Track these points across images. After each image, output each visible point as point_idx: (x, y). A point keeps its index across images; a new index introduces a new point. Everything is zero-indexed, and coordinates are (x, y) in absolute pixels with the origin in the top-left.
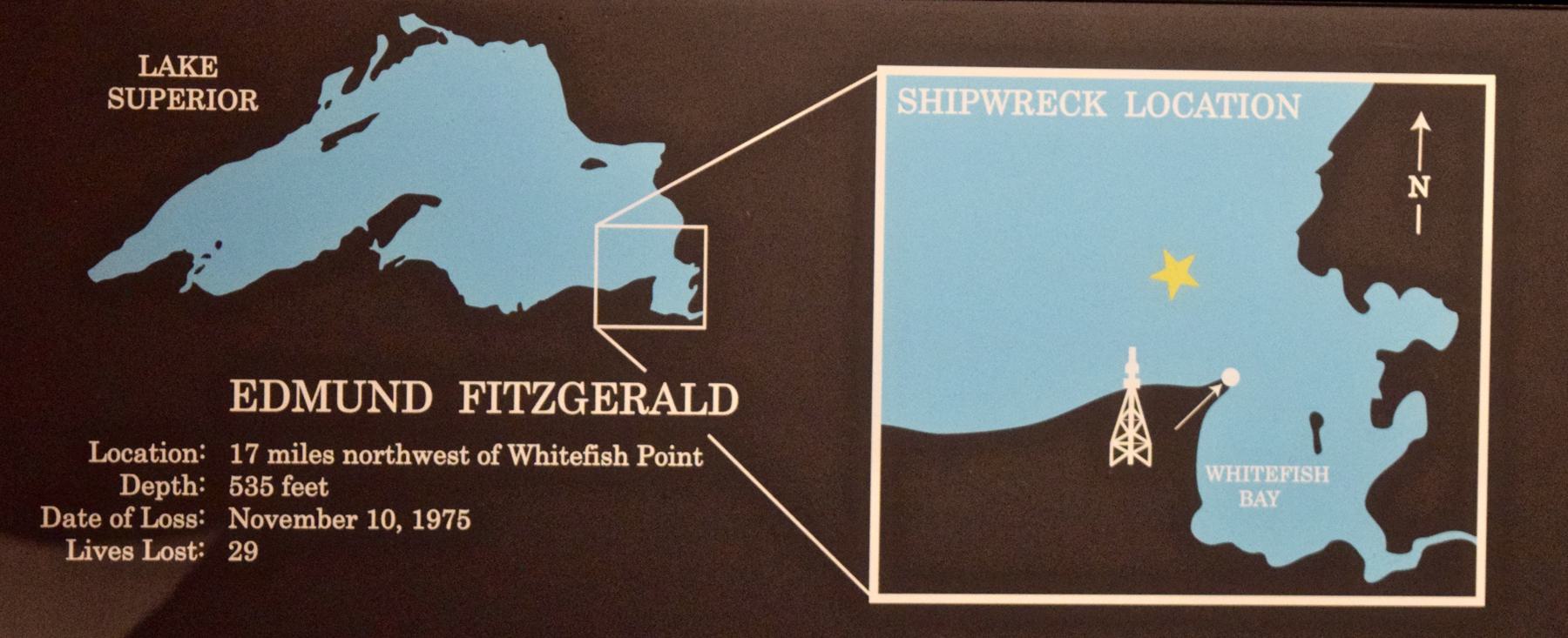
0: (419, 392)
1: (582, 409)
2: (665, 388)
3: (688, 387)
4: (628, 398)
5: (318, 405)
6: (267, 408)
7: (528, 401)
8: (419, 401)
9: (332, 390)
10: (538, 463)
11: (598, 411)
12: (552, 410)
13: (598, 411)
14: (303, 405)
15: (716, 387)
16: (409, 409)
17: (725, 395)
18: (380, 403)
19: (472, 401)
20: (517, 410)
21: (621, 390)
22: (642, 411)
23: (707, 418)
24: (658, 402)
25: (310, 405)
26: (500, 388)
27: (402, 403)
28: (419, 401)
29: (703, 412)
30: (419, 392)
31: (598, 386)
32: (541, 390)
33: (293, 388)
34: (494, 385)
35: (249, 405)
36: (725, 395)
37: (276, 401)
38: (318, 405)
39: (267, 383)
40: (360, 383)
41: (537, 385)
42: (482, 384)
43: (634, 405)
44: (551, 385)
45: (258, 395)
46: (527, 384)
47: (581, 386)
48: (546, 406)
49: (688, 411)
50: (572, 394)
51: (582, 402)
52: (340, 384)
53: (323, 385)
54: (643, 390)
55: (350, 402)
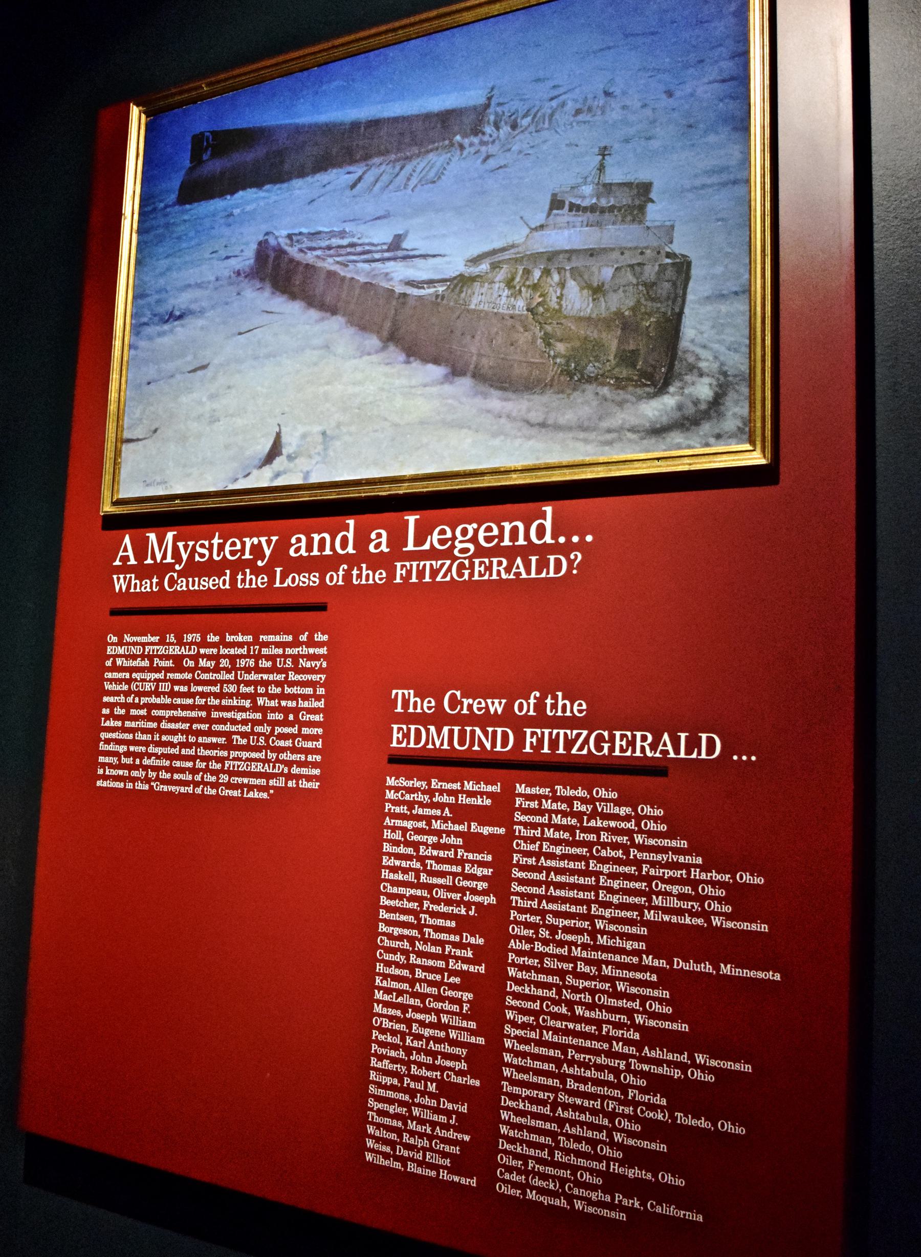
0: (505, 736)
1: (466, 577)
2: (666, 737)
3: (534, 559)
4: (495, 568)
5: (442, 744)
6: (412, 745)
7: (569, 744)
8: (505, 743)
9: (451, 732)
10: (132, 590)
11: (476, 577)
12: (585, 752)
13: (476, 577)
14: (434, 744)
15: (704, 736)
16: (498, 748)
17: (711, 742)
18: (481, 744)
19: (401, 574)
20: (427, 579)
21: (634, 737)
22: (649, 754)
23: (697, 759)
24: (514, 570)
25: (438, 744)
26: (551, 734)
27: (494, 745)
28: (505, 743)
29: (543, 575)
30: (505, 736)
31: (618, 734)
32: (442, 565)
33: (428, 731)
34: (547, 731)
35: (626, 751)
36: (711, 742)
37: (417, 741)
38: (442, 744)
39: (413, 727)
40: (468, 729)
41: (440, 562)
42: (538, 731)
43: (643, 749)
44: (585, 733)
45: (407, 736)
46: (434, 563)
47: (606, 734)
48: (445, 576)
49: (682, 755)
50: (600, 739)
51: (467, 572)
52: (456, 729)
53: (446, 729)
54: (650, 738)
55: (462, 742)
